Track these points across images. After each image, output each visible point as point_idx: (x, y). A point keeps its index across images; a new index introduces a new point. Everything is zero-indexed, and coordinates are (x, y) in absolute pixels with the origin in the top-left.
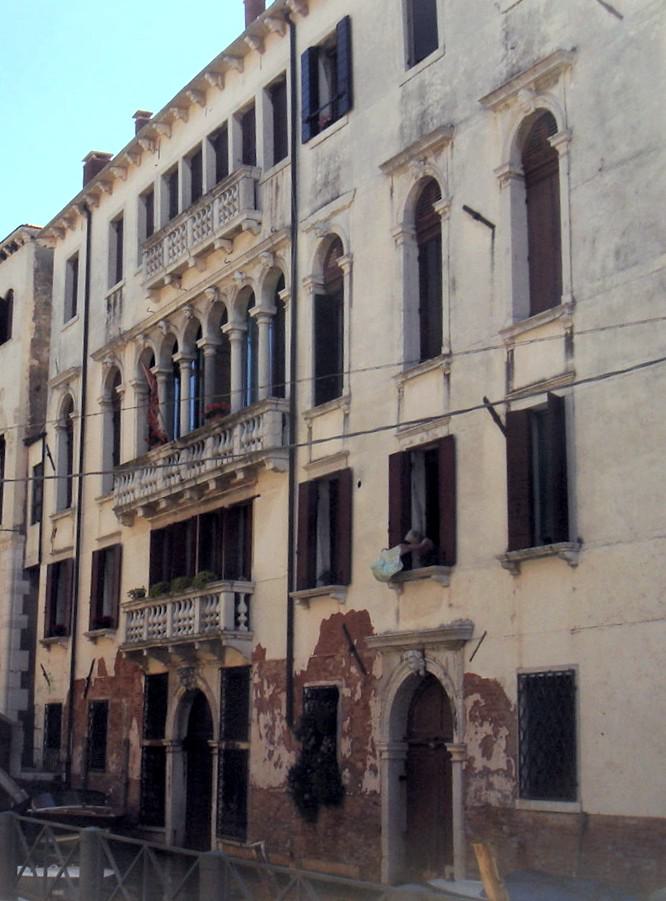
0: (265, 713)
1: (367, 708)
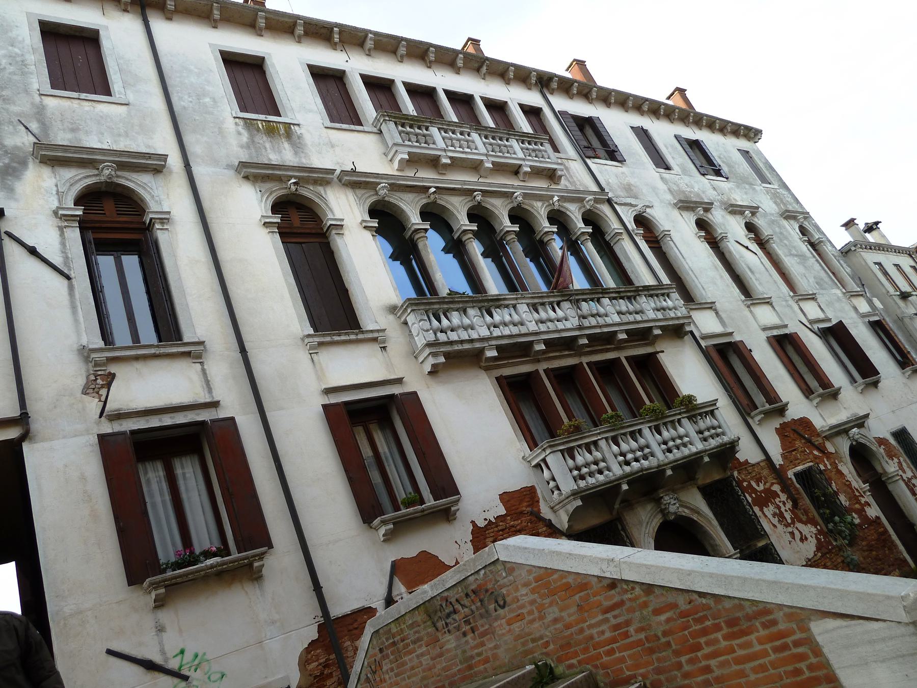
0: (767, 506)
1: (840, 473)
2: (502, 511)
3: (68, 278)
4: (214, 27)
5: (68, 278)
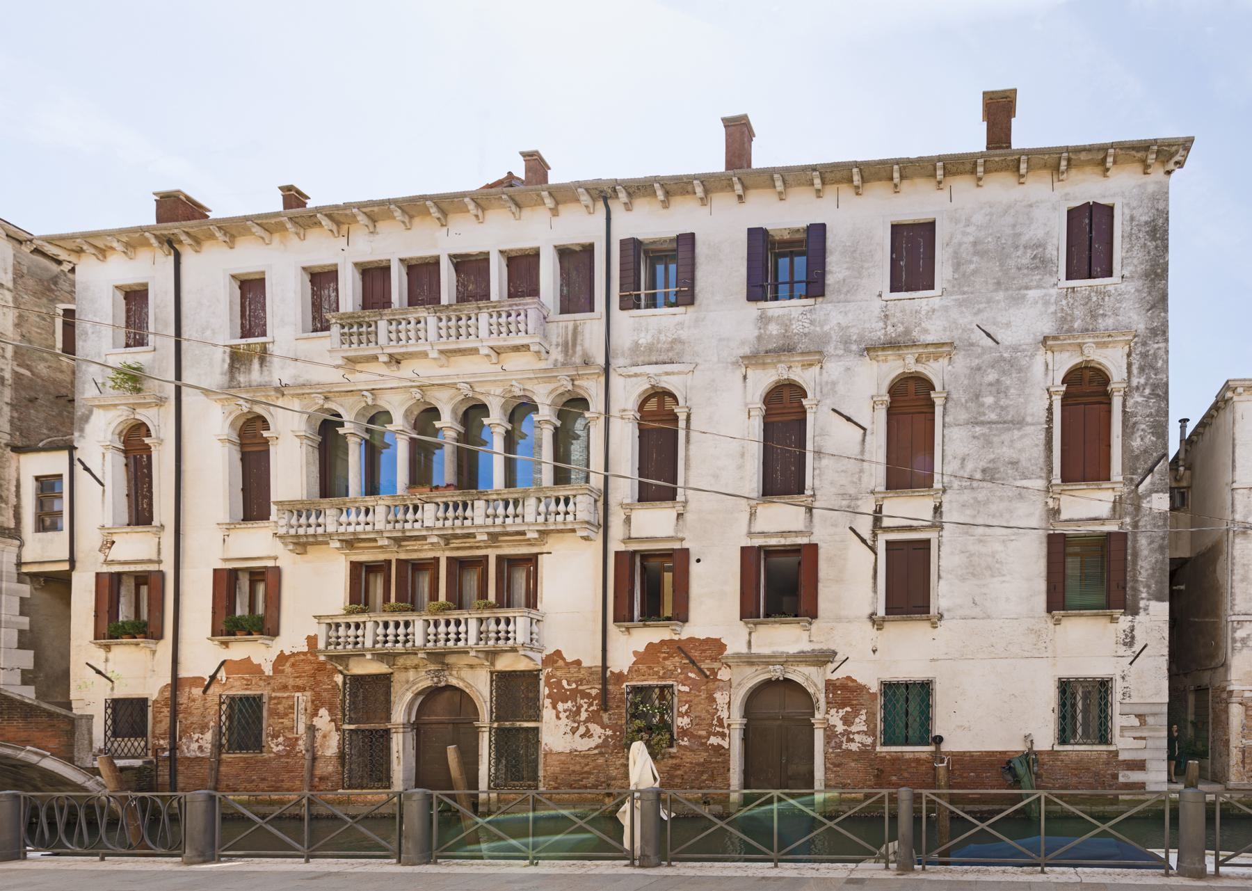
2: (306, 649)
3: (102, 484)
4: (231, 248)
5: (102, 484)
